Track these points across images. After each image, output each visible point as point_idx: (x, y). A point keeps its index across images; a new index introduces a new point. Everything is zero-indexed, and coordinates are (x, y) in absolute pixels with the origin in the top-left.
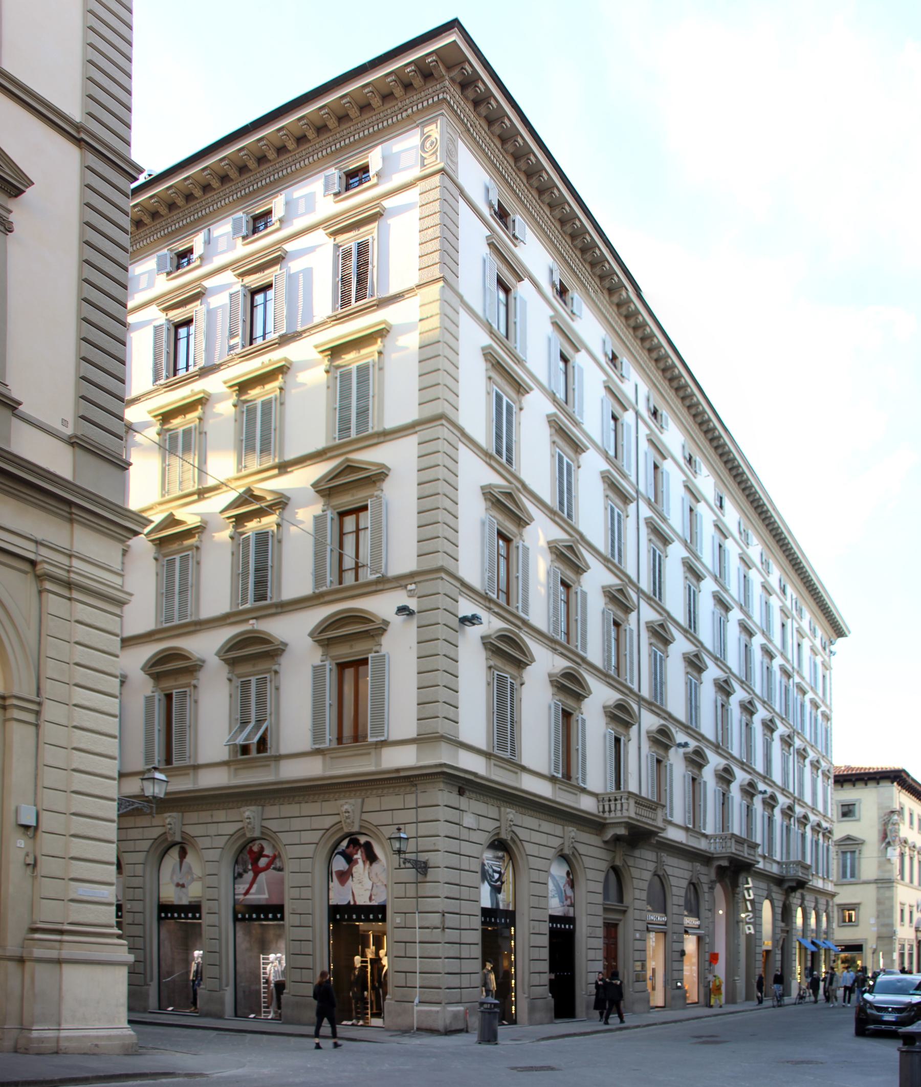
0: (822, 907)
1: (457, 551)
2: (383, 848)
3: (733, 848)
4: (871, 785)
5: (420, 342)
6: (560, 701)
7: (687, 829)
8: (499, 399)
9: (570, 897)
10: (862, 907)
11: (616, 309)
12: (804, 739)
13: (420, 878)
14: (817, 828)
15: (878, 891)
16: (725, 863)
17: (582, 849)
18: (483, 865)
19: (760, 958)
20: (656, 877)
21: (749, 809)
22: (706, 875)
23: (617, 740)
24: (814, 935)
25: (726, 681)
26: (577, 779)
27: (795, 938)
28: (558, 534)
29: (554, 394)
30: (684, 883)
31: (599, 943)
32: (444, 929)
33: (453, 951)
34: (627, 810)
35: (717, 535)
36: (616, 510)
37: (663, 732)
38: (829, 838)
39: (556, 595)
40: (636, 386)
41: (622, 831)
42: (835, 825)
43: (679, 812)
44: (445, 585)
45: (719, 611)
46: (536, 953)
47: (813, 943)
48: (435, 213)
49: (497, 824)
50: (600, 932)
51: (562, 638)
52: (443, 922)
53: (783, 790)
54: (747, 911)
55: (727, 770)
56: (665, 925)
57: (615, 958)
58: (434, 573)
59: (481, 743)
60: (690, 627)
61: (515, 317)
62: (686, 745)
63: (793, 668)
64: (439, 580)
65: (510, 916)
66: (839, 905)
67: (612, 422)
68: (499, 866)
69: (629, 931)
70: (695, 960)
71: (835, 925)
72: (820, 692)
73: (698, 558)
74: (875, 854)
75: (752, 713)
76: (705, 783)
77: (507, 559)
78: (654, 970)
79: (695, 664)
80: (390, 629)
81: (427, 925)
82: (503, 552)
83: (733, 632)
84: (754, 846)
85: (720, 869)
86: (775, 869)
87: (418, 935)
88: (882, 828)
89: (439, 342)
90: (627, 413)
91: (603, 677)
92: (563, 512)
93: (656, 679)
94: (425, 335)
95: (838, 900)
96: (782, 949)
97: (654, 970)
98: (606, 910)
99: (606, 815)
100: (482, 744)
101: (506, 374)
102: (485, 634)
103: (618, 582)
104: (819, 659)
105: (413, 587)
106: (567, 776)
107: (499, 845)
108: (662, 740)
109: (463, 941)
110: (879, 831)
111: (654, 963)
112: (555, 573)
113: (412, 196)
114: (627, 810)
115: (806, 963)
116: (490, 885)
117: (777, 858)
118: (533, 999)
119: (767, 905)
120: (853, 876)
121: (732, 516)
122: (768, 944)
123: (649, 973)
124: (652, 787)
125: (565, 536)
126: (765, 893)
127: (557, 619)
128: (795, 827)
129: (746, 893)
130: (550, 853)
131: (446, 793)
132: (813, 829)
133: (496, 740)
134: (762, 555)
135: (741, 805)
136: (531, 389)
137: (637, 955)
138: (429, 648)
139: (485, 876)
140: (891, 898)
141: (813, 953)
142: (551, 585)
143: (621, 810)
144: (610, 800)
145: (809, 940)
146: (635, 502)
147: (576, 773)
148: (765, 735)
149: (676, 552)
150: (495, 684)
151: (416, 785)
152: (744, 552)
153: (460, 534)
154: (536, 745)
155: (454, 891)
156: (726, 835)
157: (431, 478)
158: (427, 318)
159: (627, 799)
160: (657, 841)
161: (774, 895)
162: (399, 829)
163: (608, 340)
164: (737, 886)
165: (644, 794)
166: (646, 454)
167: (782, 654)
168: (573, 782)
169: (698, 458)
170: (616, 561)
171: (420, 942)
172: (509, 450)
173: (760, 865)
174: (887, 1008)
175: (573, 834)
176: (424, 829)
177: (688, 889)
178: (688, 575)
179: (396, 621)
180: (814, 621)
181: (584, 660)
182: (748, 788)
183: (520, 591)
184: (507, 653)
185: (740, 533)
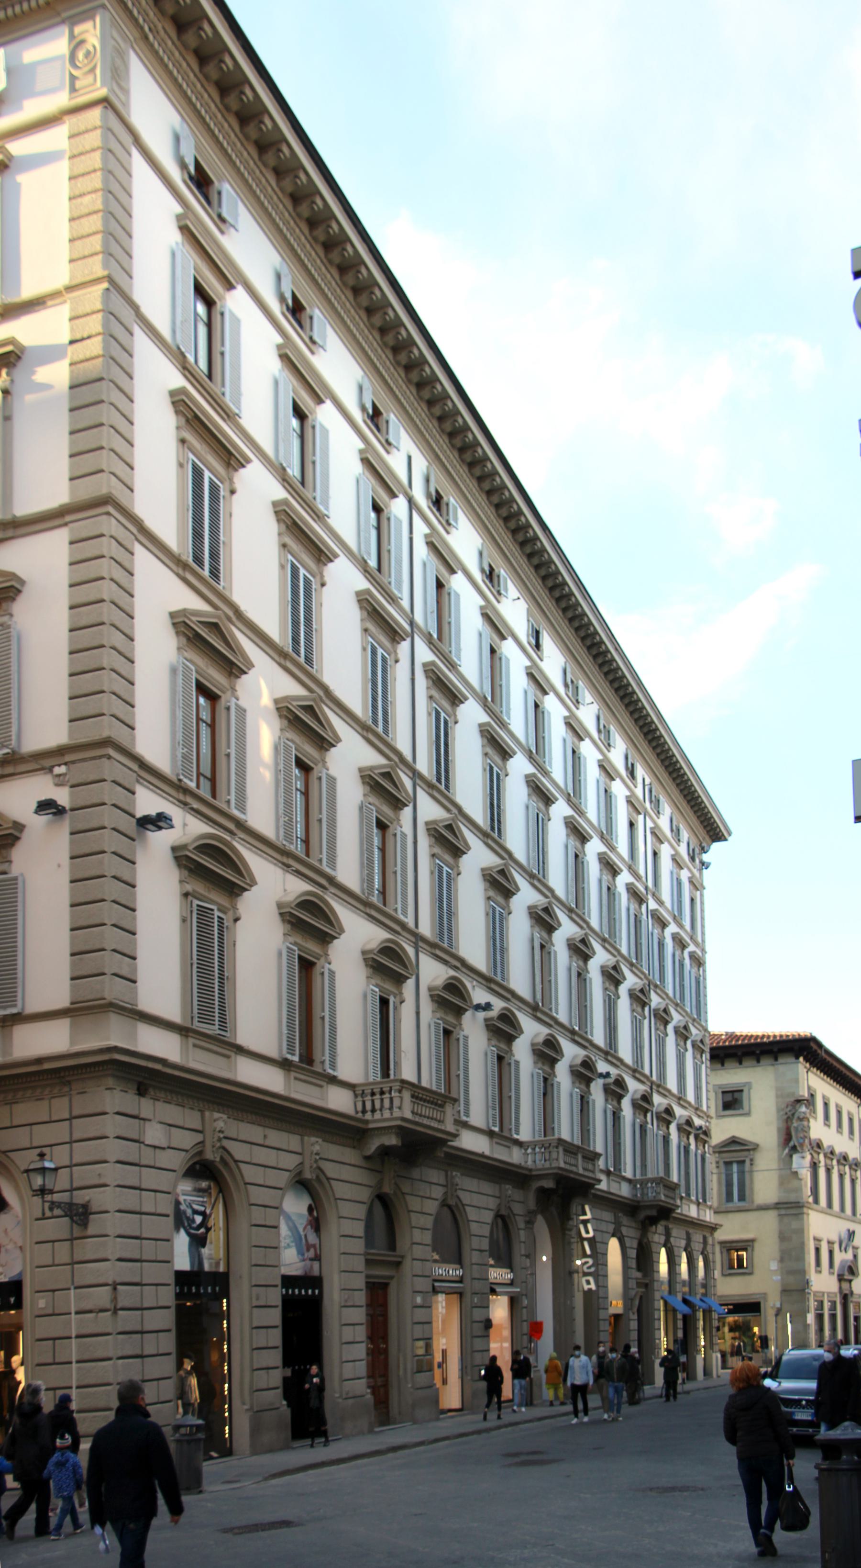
0: (697, 1246)
1: (133, 714)
2: (17, 1188)
3: (561, 1161)
4: (766, 1061)
5: (72, 378)
6: (295, 944)
7: (490, 1134)
8: (198, 475)
9: (314, 1246)
10: (756, 1245)
11: (378, 337)
12: (664, 995)
13: (77, 1232)
14: (686, 1127)
15: (781, 1221)
16: (549, 1184)
17: (331, 1170)
18: (178, 1203)
19: (606, 1327)
20: (446, 1208)
21: (584, 1102)
22: (521, 1203)
23: (384, 1002)
24: (686, 1289)
25: (546, 910)
26: (323, 1062)
27: (657, 1295)
28: (291, 688)
29: (284, 469)
30: (488, 1217)
31: (359, 1315)
32: (115, 1311)
33: (130, 1345)
34: (400, 1108)
35: (532, 690)
36: (380, 651)
37: (453, 987)
38: (705, 1142)
39: (288, 782)
40: (410, 458)
41: (392, 1140)
42: (714, 1121)
43: (478, 1107)
44: (114, 768)
45: (536, 804)
46: (261, 1338)
47: (685, 1301)
48: (95, 171)
49: (199, 1138)
50: (361, 1298)
51: (297, 848)
52: (115, 1299)
53: (635, 1071)
54: (585, 1255)
55: (551, 1043)
56: (461, 1281)
57: (385, 1338)
58: (97, 747)
59: (172, 1011)
60: (493, 829)
61: (223, 345)
62: (488, 1007)
63: (646, 888)
64: (104, 760)
65: (220, 1283)
66: (722, 1243)
67: (373, 515)
68: (202, 1204)
69: (405, 1294)
70: (507, 1333)
71: (717, 1274)
72: (687, 924)
73: (504, 725)
74: (774, 1165)
75: (586, 958)
76: (517, 1063)
77: (212, 726)
78: (444, 1352)
79: (499, 885)
80: (26, 836)
81: (88, 1307)
82: (205, 715)
83: (557, 835)
84: (593, 1157)
85: (543, 1193)
86: (625, 1191)
87: (75, 1323)
88: (783, 1125)
89: (101, 379)
90: (396, 500)
91: (361, 907)
92: (298, 654)
93: (441, 908)
94: (79, 366)
95: (721, 1235)
96: (639, 1311)
97: (444, 1352)
98: (369, 1263)
99: (368, 1116)
100: (174, 1014)
101: (210, 437)
102: (177, 843)
103: (383, 761)
104: (685, 875)
105: (62, 769)
106: (308, 1058)
107: (205, 1170)
108: (451, 1000)
109: (146, 1328)
110: (779, 1130)
111: (444, 1341)
112: (287, 749)
113: (56, 138)
114: (400, 1108)
115: (675, 1333)
116: (189, 1234)
117: (628, 1173)
118: (257, 1415)
119: (614, 1245)
120: (742, 1198)
121: (554, 661)
122: (617, 1305)
123: (438, 1358)
124: (438, 1071)
125: (300, 691)
126: (611, 1228)
127: (291, 820)
128: (653, 1127)
129: (582, 1228)
130: (283, 1179)
131: (117, 1094)
132: (680, 1129)
133: (196, 1007)
134: (598, 718)
135: (571, 1095)
136: (248, 461)
137: (418, 1331)
138: (90, 866)
139: (180, 1220)
140: (801, 1232)
141: (685, 1318)
142: (281, 767)
143: (391, 1108)
144: (373, 1094)
145: (679, 1297)
146: (409, 640)
147: (322, 1054)
148: (606, 989)
149: (471, 715)
150: (195, 920)
151: (69, 1082)
152: (573, 715)
153: (137, 643)
154: (259, 1012)
155: (131, 1248)
156: (549, 1142)
157: (92, 598)
158: (83, 339)
159: (400, 1091)
160: (447, 1155)
161: (624, 1230)
162: (42, 1155)
163: (367, 385)
164: (569, 1218)
165: (425, 1083)
166: (425, 565)
167: (630, 868)
168: (317, 1068)
169: (502, 572)
170: (380, 729)
171: (78, 1337)
172: (214, 556)
173: (603, 1186)
174: (800, 1400)
175: (317, 1148)
176: (82, 1152)
177: (494, 1224)
178: (489, 750)
179: (36, 823)
180: (677, 818)
181: (332, 881)
182: (582, 1070)
183: (233, 777)
184: (213, 872)
185: (566, 685)
